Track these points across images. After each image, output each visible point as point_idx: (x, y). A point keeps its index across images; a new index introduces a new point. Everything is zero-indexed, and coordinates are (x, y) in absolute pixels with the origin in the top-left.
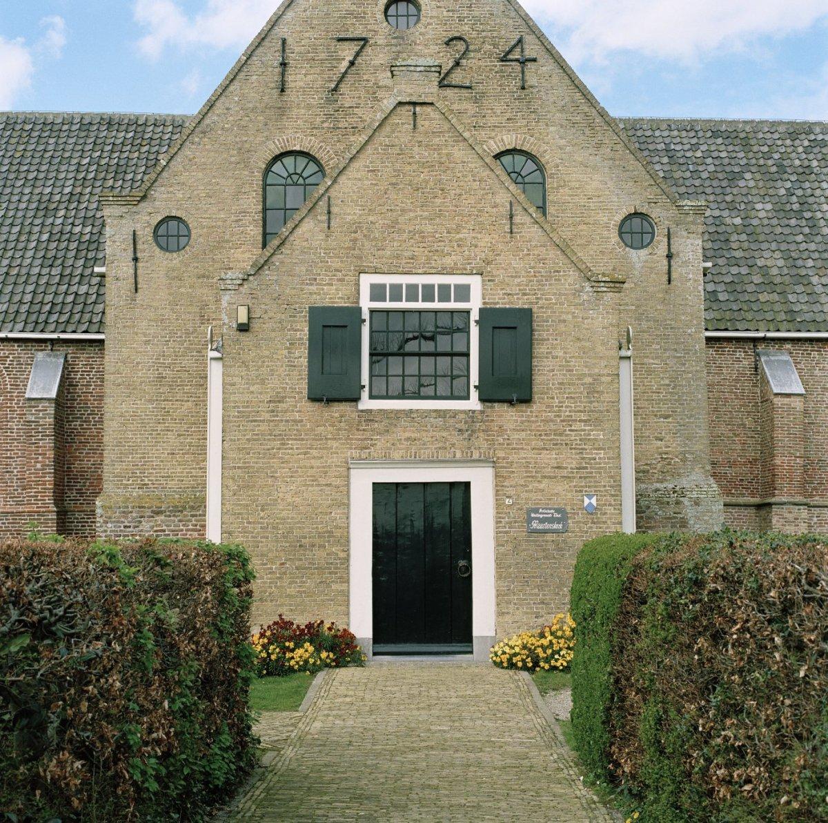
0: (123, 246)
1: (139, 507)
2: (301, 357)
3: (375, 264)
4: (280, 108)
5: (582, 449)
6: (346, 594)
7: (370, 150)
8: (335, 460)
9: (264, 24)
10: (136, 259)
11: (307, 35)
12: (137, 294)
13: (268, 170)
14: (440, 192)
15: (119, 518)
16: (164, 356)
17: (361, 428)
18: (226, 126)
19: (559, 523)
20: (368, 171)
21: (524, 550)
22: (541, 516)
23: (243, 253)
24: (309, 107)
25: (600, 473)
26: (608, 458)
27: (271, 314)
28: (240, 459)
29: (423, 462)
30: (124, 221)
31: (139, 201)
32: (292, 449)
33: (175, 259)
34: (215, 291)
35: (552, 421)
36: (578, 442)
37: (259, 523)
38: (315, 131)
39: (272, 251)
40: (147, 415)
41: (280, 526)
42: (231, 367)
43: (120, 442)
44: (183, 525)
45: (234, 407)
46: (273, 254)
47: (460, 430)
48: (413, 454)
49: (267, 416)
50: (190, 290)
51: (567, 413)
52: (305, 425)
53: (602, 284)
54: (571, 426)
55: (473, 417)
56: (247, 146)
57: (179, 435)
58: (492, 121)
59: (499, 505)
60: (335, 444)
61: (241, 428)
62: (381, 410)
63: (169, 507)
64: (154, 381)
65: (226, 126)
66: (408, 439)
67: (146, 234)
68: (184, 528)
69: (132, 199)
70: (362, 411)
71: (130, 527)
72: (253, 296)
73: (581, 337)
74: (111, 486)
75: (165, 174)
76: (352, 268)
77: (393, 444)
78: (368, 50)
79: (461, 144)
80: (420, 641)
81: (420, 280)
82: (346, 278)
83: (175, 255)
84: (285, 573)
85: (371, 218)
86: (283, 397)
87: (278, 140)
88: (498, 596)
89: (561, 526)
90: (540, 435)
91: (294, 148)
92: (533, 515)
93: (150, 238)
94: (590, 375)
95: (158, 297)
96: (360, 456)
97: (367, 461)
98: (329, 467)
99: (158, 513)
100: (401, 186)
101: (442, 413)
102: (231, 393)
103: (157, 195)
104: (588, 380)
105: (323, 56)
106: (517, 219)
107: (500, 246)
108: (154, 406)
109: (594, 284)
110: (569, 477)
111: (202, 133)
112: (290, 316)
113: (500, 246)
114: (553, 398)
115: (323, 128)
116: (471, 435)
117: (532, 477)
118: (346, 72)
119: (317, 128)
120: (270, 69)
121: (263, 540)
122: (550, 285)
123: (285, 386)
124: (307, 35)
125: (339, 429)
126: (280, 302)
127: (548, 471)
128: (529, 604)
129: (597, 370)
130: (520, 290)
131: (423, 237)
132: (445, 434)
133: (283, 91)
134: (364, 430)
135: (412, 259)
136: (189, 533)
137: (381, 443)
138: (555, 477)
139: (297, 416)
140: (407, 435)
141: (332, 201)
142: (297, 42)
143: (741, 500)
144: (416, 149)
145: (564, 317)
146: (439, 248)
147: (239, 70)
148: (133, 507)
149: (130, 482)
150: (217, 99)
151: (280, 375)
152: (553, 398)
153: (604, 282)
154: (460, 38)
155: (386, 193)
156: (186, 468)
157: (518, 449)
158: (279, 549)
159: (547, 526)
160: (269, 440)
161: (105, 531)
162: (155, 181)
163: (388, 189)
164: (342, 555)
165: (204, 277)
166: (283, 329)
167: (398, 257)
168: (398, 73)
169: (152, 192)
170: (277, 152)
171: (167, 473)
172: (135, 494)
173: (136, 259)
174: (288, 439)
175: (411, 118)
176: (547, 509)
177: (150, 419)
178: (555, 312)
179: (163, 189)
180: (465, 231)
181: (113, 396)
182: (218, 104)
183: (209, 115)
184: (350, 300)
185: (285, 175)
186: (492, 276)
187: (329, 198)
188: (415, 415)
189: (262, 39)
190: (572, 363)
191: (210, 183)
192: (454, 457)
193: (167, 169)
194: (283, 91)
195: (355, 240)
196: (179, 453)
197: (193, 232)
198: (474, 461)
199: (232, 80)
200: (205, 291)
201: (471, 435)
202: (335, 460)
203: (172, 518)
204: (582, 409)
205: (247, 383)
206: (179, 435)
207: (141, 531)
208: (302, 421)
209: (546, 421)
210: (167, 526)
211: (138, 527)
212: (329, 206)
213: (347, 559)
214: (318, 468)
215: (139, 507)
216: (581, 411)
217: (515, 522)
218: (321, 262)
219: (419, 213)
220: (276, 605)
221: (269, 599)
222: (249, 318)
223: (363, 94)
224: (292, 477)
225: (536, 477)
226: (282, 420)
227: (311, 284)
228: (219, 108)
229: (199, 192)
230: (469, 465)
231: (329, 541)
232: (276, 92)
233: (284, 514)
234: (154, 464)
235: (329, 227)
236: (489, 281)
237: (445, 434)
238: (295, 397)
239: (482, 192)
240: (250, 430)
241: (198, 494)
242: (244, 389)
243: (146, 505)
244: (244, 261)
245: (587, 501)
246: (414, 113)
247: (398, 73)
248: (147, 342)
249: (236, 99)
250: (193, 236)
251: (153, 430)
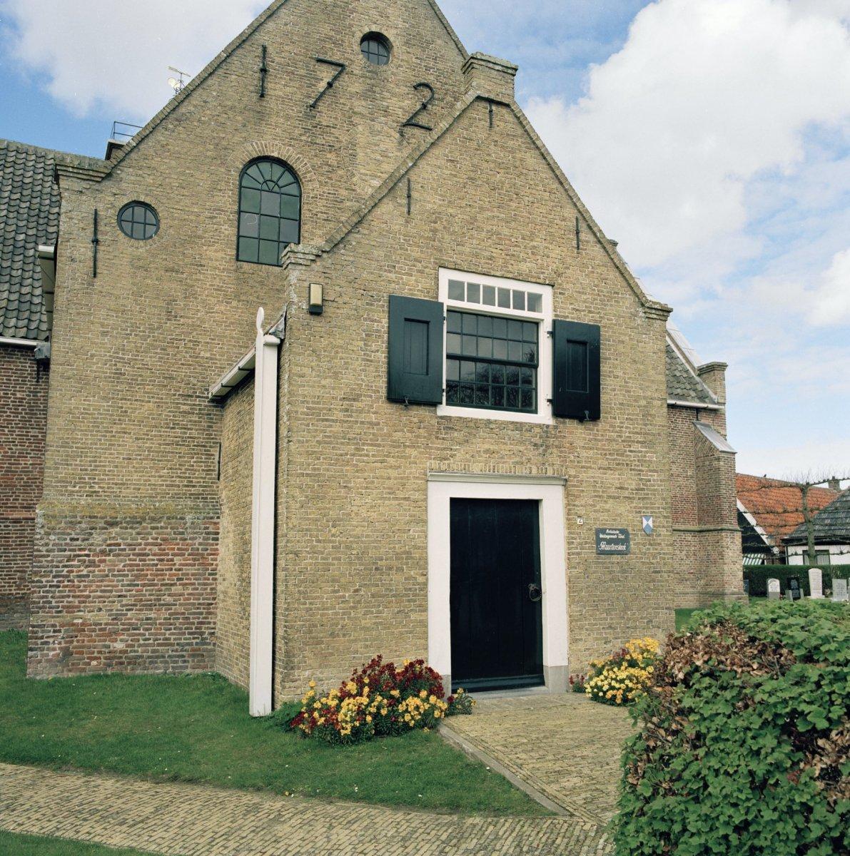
0: (82, 225)
1: (90, 517)
2: (378, 351)
3: (455, 260)
4: (259, 112)
5: (640, 470)
6: (424, 624)
7: (448, 139)
8: (414, 471)
9: (246, 27)
10: (96, 241)
11: (286, 48)
12: (96, 280)
13: (243, 173)
14: (515, 196)
15: (64, 529)
16: (123, 350)
17: (441, 436)
18: (203, 119)
19: (623, 545)
20: (447, 160)
21: (594, 572)
22: (608, 537)
23: (216, 251)
24: (288, 118)
25: (654, 495)
26: (661, 481)
27: (346, 299)
28: (309, 465)
29: (502, 476)
30: (84, 198)
31: (103, 178)
32: (367, 455)
33: (142, 248)
34: (185, 287)
35: (614, 440)
36: (637, 463)
37: (330, 541)
38: (293, 142)
39: (350, 228)
40: (101, 414)
41: (354, 546)
42: (299, 354)
43: (67, 443)
44: (142, 539)
45: (303, 402)
46: (350, 232)
47: (535, 445)
48: (492, 468)
49: (340, 415)
50: (157, 282)
51: (627, 434)
52: (382, 429)
53: (654, 311)
54: (630, 446)
55: (547, 432)
56: (224, 143)
57: (137, 439)
59: (570, 524)
60: (414, 453)
61: (311, 427)
62: (461, 418)
63: (125, 518)
64: (110, 377)
65: (203, 119)
66: (487, 451)
67: (109, 217)
68: (143, 542)
69: (95, 174)
70: (442, 417)
71: (77, 539)
72: (326, 275)
73: (637, 359)
74: (53, 492)
75: (133, 155)
76: (432, 260)
77: (472, 456)
78: (345, 77)
79: (533, 152)
80: (486, 676)
82: (427, 270)
83: (141, 243)
84: (359, 602)
85: (451, 211)
86: (358, 395)
87: (256, 143)
88: (571, 622)
89: (624, 547)
90: (605, 454)
91: (272, 154)
92: (601, 536)
93: (113, 221)
94: (645, 398)
95: (119, 285)
96: (440, 467)
97: (445, 475)
98: (408, 478)
99: (113, 524)
100: (479, 182)
101: (518, 425)
102: (300, 386)
103: (123, 175)
104: (643, 403)
105: (302, 72)
106: (583, 236)
107: (569, 260)
108: (110, 404)
109: (647, 310)
110: (630, 498)
111: (177, 120)
112: (367, 304)
113: (569, 260)
114: (615, 418)
115: (301, 141)
116: (545, 451)
117: (600, 497)
118: (323, 94)
119: (295, 139)
120: (250, 73)
121: (336, 562)
122: (611, 305)
123: (360, 382)
124: (286, 48)
125: (418, 437)
126: (356, 285)
127: (613, 492)
128: (599, 629)
129: (650, 394)
130: (586, 307)
131: (500, 239)
132: (522, 448)
133: (262, 96)
134: (443, 439)
135: (491, 259)
136: (148, 547)
137: (461, 453)
138: (619, 497)
139: (373, 418)
140: (487, 446)
141: (412, 186)
142: (277, 53)
143: (683, 527)
144: (492, 147)
145: (622, 338)
146: (515, 253)
147: (219, 66)
148: (82, 517)
149: (77, 488)
150: (194, 89)
151: (355, 370)
152: (615, 418)
153: (655, 309)
154: (426, 85)
155: (465, 187)
156: (144, 476)
157: (587, 468)
158: (353, 573)
159: (613, 547)
160: (342, 443)
161: (47, 544)
162: (122, 160)
163: (466, 183)
164: (421, 579)
165: (173, 271)
166: (359, 318)
167: (477, 256)
168: (478, 67)
169: (119, 172)
170: (255, 155)
171: (122, 480)
172: (83, 502)
173: (96, 241)
174: (363, 444)
175: (488, 116)
176: (612, 530)
177: (104, 418)
178: (615, 333)
179: (131, 170)
180: (537, 239)
181: (61, 390)
182: (196, 95)
183: (185, 104)
184: (430, 294)
185: (261, 180)
186: (563, 289)
187: (409, 181)
188: (494, 426)
189: (243, 41)
190: (630, 385)
191: (183, 173)
192: (530, 473)
193: (136, 150)
194: (262, 96)
195: (435, 231)
196: (136, 459)
197: (163, 221)
198: (549, 478)
199: (210, 74)
200: (173, 286)
201: (545, 451)
202: (414, 471)
203: (129, 530)
204: (638, 430)
205: (318, 376)
206: (137, 439)
207: (92, 545)
208: (378, 424)
209: (610, 440)
210: (123, 539)
211: (87, 540)
212: (409, 190)
213: (426, 584)
214: (396, 479)
215: (90, 517)
216: (637, 433)
217: (586, 543)
218: (401, 249)
219: (496, 214)
220: (349, 641)
221: (341, 633)
222: (323, 300)
223: (339, 116)
224: (367, 488)
225: (603, 497)
226: (357, 422)
227: (390, 272)
228: (196, 99)
229: (171, 180)
230: (543, 482)
231: (407, 564)
232: (255, 97)
233: (358, 531)
234: (107, 469)
235: (409, 212)
236: (560, 293)
237: (522, 448)
238: (371, 396)
239: (552, 204)
240: (322, 431)
241: (157, 504)
242: (314, 382)
243: (99, 515)
244: (217, 260)
245: (645, 523)
246: (491, 111)
247: (478, 67)
248: (104, 334)
249: (215, 94)
250: (162, 226)
251: (106, 432)
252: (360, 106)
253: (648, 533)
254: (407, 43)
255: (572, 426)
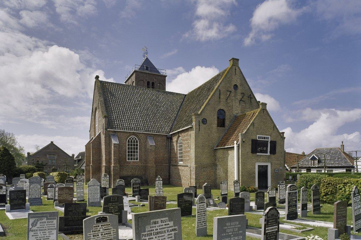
6: (255, 181)
10: (199, 125)
33: (205, 126)
58: (247, 107)
59: (271, 168)
67: (201, 121)
81: (264, 136)
137: (259, 159)
252: (233, 98)
253: (281, 169)
254: (240, 86)
255: (272, 155)
